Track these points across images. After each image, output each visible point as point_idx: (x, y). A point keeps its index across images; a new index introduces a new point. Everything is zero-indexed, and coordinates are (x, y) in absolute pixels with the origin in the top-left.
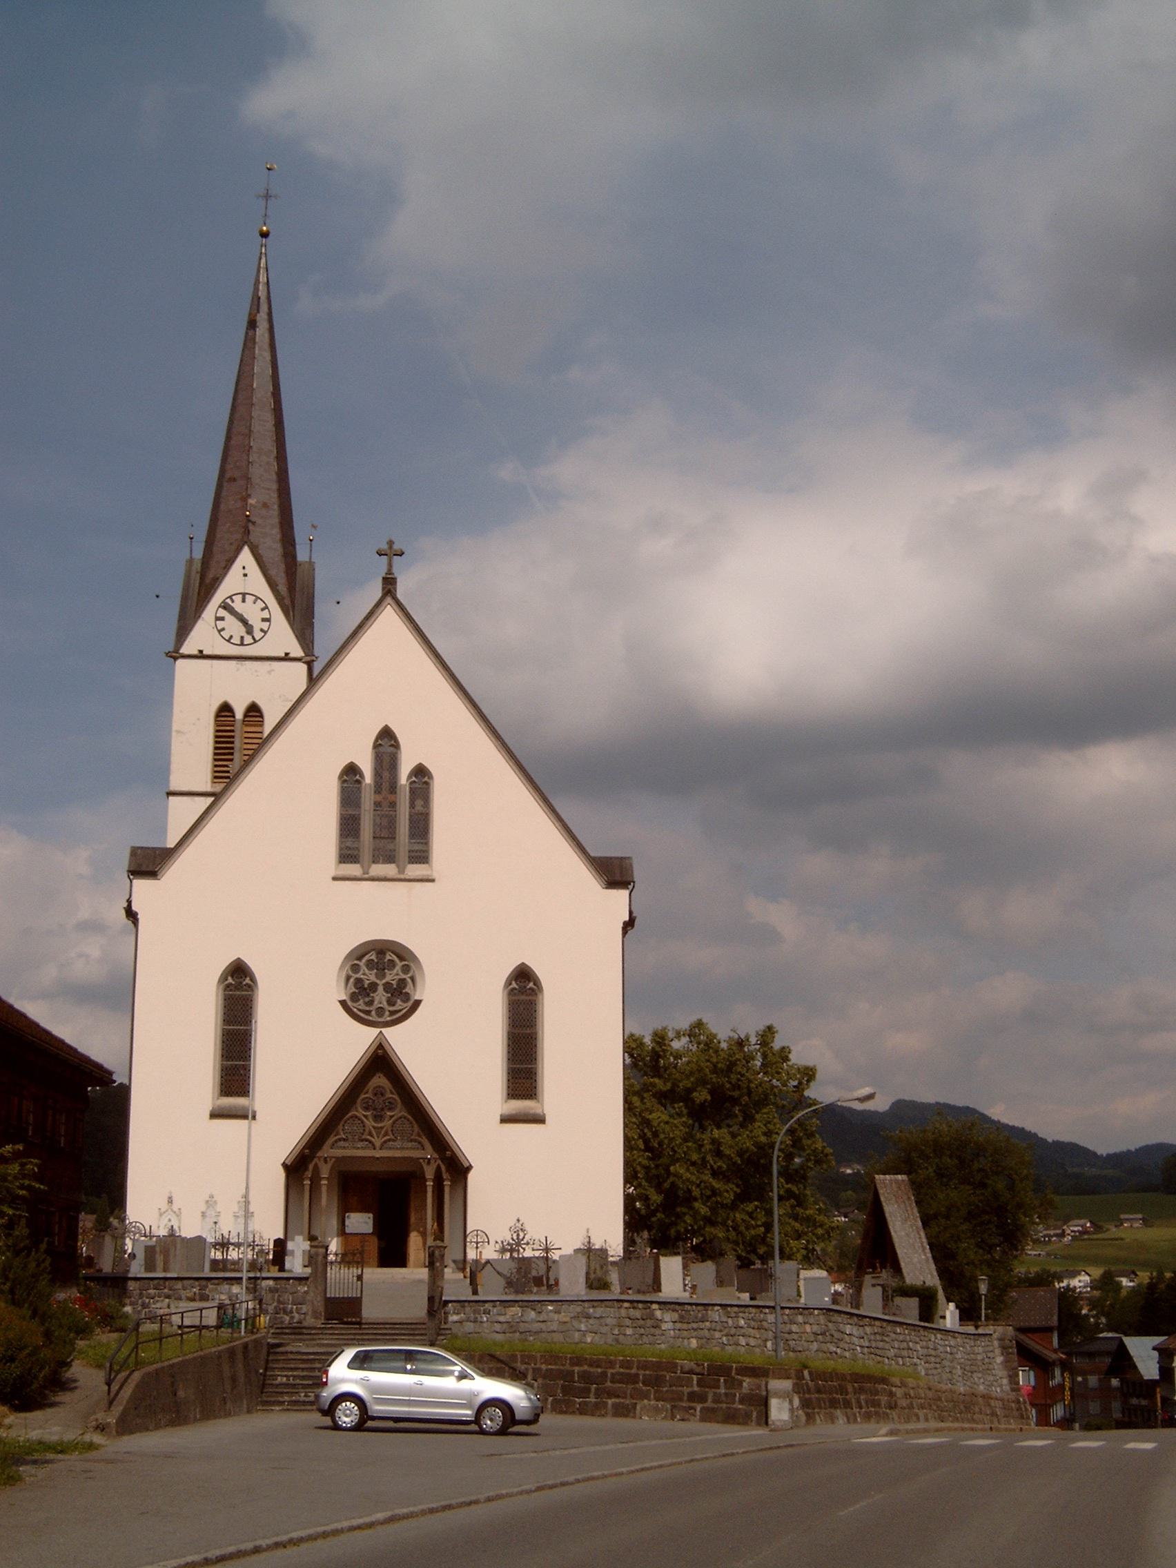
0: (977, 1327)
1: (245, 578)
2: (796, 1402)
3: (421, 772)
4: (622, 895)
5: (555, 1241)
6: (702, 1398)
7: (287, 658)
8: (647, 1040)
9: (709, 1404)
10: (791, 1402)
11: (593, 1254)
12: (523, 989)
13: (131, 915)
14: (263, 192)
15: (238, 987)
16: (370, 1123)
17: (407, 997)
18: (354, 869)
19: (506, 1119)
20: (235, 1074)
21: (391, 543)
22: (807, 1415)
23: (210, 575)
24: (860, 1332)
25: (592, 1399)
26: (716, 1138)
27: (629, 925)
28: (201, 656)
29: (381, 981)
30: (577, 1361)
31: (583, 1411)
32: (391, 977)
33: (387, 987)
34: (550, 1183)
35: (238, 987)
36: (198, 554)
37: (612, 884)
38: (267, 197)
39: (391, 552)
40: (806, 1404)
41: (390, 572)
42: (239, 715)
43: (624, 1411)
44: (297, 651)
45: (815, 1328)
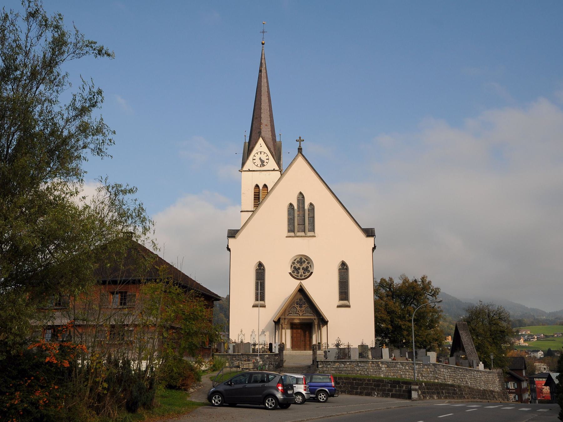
0: (490, 369)
1: (261, 146)
2: (420, 392)
3: (311, 204)
4: (371, 239)
5: (351, 344)
6: (391, 391)
7: (274, 170)
8: (387, 280)
9: (394, 392)
10: (418, 392)
11: (363, 348)
12: (344, 268)
13: (229, 249)
14: (262, 31)
15: (260, 271)
16: (298, 308)
17: (309, 271)
18: (292, 234)
19: (338, 307)
20: (260, 295)
21: (300, 138)
22: (423, 396)
23: (251, 147)
24: (446, 371)
25: (359, 390)
26: (403, 310)
27: (374, 248)
28: (249, 171)
29: (302, 267)
30: (354, 379)
31: (356, 394)
32: (304, 265)
33: (303, 269)
34: (352, 326)
35: (260, 271)
36: (247, 141)
37: (368, 236)
38: (263, 32)
39: (300, 140)
40: (423, 393)
41: (300, 146)
42: (261, 187)
43: (369, 394)
44: (277, 168)
45: (431, 370)
